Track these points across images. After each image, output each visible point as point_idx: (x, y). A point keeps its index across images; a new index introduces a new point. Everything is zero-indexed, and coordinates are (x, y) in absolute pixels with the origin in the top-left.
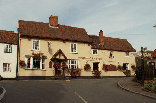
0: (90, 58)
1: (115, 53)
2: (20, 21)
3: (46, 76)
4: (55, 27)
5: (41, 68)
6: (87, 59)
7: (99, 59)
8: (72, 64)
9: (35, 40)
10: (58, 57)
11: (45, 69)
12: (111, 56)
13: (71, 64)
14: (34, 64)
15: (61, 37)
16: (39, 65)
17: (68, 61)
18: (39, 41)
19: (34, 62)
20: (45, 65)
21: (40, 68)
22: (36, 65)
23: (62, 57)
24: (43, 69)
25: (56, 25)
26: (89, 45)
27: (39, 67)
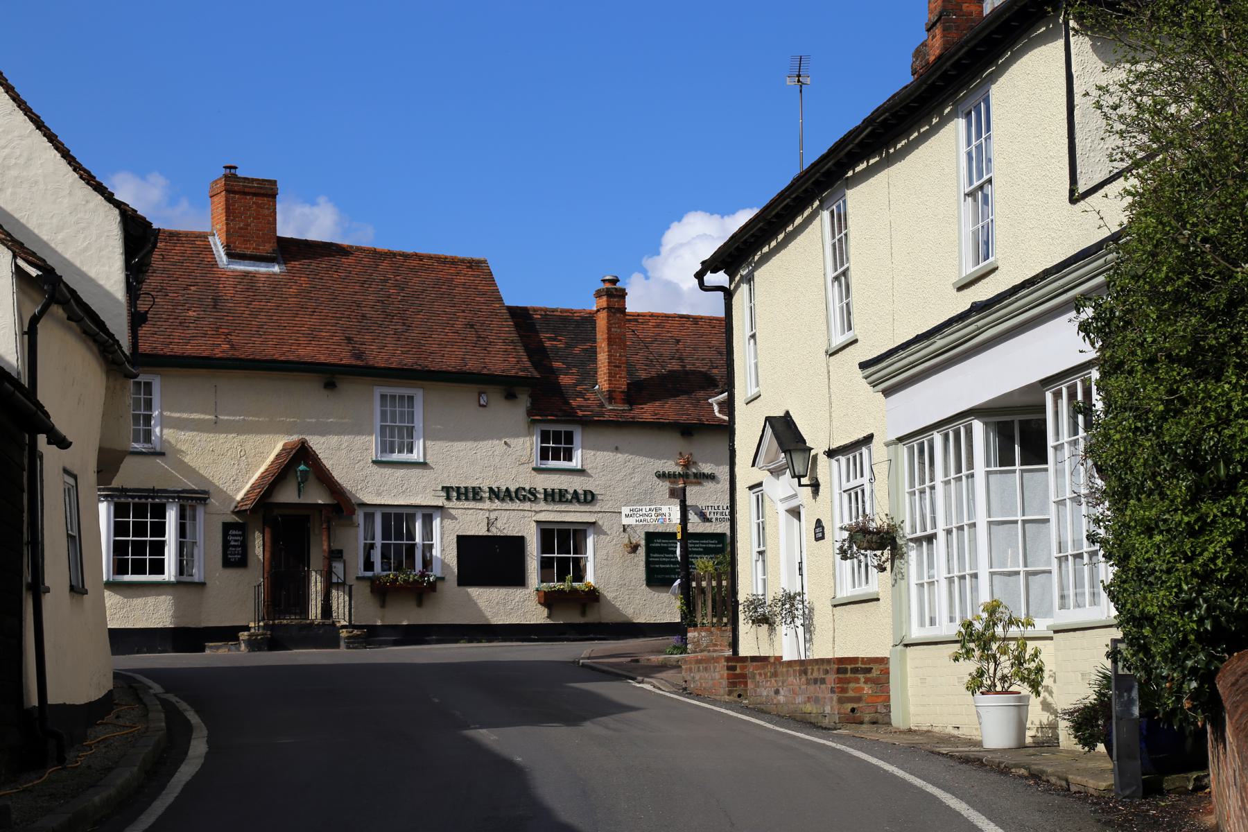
0: (513, 489)
1: (482, 531)
2: (787, 412)
3: (203, 625)
4: (263, 269)
5: (170, 573)
6: (497, 504)
7: (589, 498)
8: (386, 535)
9: (389, 391)
10: (288, 495)
11: (196, 579)
12: (186, 710)
13: (378, 541)
14: (119, 548)
15: (306, 352)
16: (159, 548)
17: (360, 517)
18: (411, 398)
19: (120, 529)
20: (199, 553)
21: (162, 572)
22: (139, 548)
23: (319, 497)
24: (185, 578)
25: (267, 248)
26: (510, 396)
27: (158, 568)
